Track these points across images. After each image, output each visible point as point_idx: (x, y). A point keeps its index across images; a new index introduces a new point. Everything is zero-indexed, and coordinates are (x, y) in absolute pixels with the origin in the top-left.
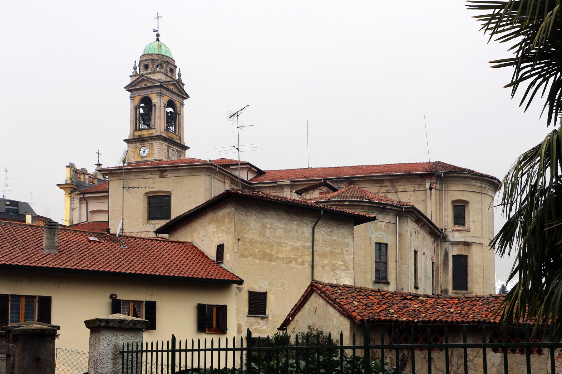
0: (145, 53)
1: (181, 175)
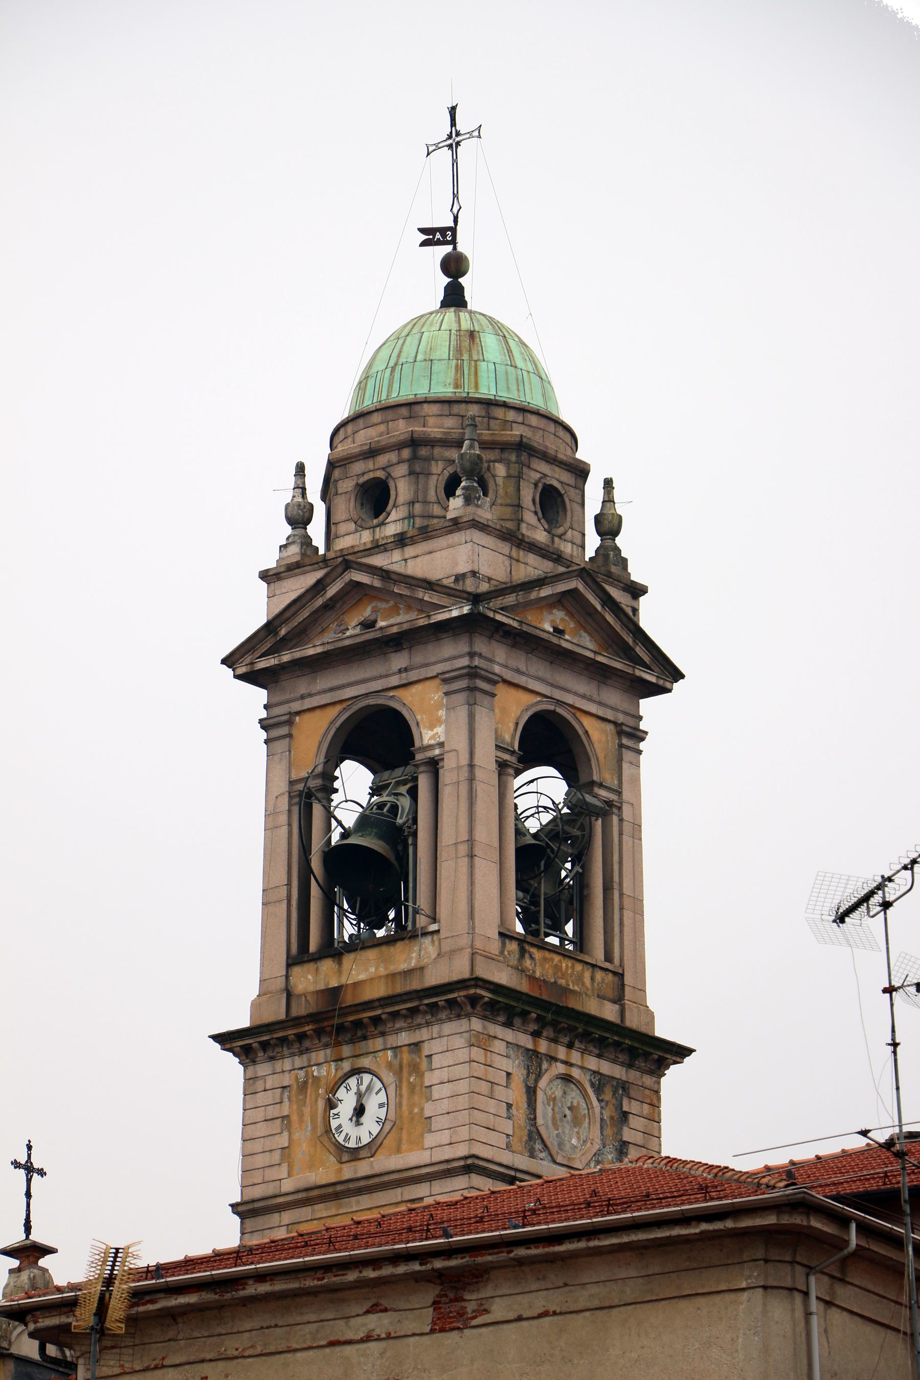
0: (368, 403)
1: (583, 1298)
